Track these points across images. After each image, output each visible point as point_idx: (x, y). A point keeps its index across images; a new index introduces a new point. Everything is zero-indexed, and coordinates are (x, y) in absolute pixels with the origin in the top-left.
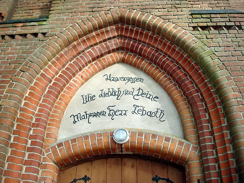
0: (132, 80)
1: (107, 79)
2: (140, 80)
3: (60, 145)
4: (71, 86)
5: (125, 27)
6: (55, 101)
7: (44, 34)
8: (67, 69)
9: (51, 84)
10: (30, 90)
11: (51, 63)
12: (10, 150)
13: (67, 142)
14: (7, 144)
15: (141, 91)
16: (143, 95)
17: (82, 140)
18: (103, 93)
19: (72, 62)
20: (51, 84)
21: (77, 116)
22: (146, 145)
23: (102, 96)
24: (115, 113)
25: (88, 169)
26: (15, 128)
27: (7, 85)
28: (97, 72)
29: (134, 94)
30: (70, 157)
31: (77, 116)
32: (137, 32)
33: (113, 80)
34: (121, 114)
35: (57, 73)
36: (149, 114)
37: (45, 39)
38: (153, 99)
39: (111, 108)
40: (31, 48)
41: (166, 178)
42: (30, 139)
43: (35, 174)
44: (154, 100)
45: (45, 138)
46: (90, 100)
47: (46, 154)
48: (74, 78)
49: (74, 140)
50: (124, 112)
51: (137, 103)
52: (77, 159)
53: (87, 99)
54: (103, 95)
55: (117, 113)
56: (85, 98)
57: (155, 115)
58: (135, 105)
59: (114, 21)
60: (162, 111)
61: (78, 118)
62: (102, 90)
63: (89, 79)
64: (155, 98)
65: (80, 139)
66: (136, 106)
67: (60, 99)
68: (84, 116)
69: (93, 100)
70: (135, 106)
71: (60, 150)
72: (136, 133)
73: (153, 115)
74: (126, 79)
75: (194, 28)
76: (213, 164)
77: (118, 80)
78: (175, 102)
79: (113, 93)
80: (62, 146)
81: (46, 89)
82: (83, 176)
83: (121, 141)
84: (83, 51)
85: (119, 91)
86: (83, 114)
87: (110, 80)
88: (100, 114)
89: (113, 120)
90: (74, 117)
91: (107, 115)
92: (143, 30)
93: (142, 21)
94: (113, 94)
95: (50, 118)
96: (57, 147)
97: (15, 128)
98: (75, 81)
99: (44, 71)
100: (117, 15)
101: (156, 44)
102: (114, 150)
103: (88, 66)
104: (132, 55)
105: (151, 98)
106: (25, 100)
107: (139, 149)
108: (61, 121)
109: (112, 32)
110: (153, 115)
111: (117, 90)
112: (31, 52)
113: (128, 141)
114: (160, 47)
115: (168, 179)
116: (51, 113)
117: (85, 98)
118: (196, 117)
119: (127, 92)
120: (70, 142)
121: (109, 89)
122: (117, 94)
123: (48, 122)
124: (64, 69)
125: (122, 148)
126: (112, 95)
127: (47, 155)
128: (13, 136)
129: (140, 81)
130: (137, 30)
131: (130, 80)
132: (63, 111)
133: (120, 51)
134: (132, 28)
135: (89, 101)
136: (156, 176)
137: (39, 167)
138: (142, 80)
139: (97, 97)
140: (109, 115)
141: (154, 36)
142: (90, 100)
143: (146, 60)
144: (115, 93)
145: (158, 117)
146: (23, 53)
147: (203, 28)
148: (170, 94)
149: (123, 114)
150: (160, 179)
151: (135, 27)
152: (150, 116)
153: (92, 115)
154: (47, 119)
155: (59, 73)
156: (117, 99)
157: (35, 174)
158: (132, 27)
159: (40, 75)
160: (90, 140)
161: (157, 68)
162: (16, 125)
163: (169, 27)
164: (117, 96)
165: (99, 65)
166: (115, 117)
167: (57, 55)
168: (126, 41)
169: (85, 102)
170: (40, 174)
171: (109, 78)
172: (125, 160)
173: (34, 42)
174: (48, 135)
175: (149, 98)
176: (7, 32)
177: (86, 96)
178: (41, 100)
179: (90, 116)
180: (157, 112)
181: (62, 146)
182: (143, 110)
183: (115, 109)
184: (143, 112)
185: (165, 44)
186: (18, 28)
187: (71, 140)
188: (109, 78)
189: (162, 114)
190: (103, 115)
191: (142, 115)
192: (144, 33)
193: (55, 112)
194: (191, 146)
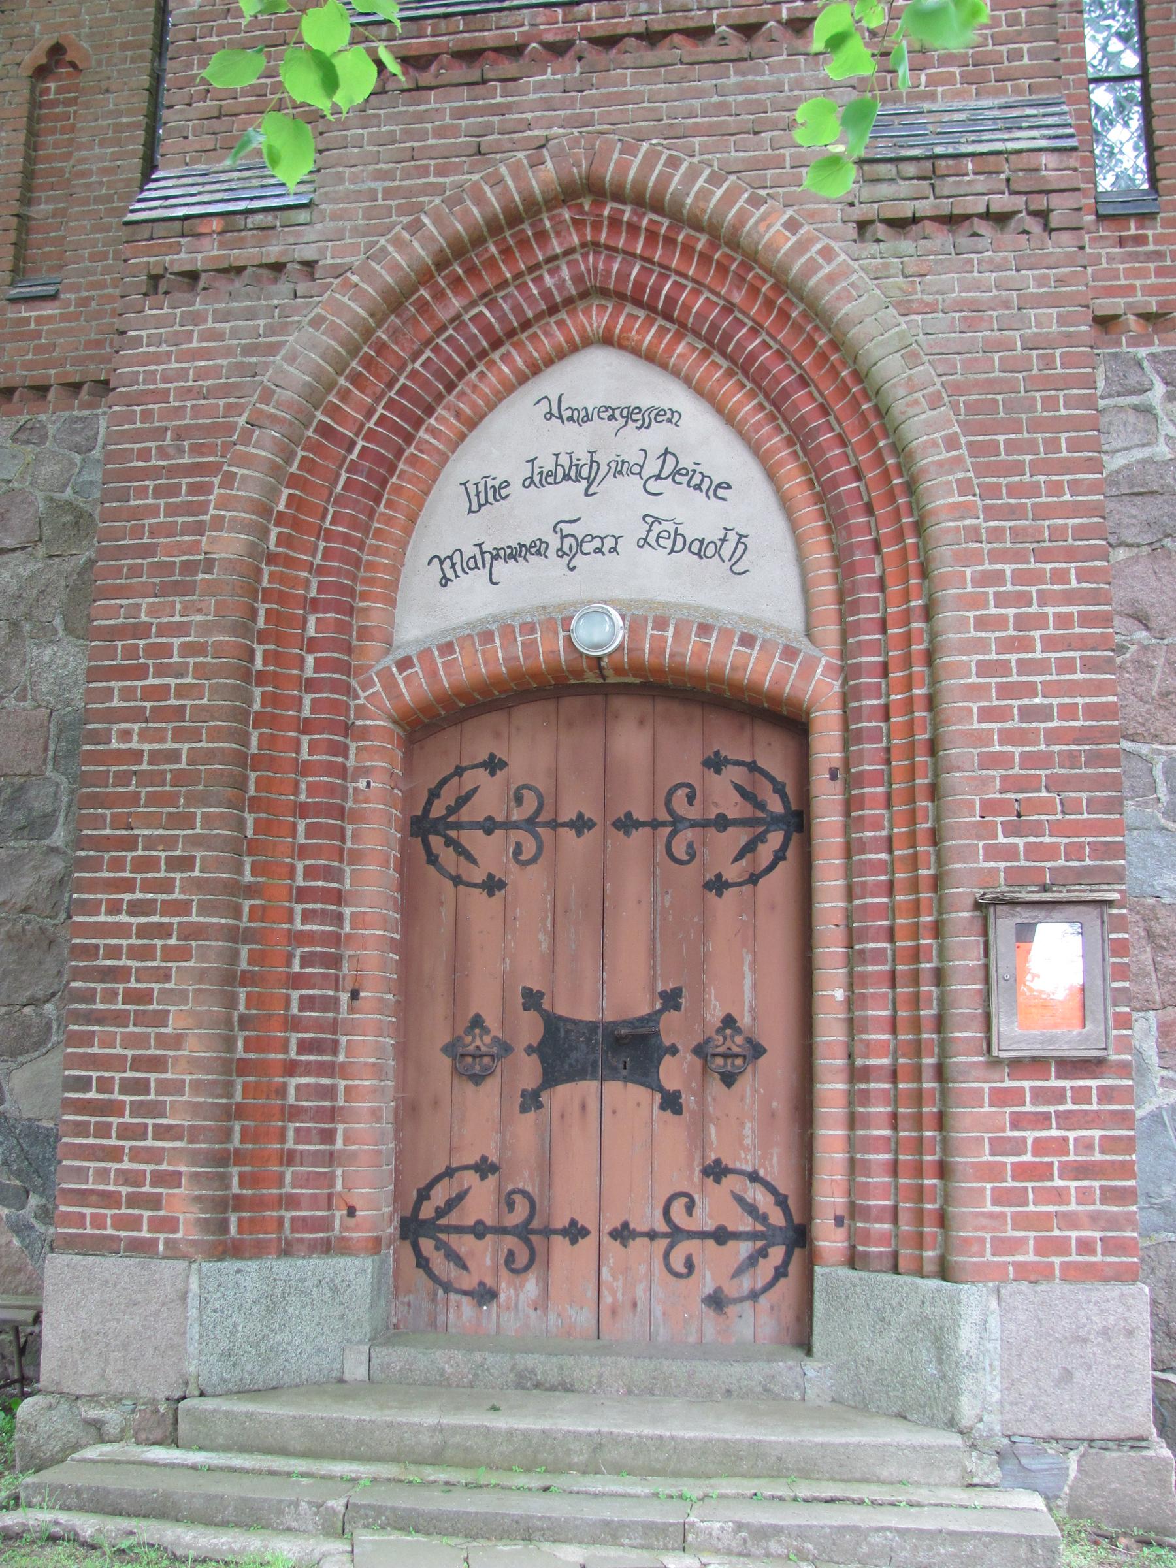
0: (639, 417)
1: (549, 415)
2: (669, 415)
3: (404, 664)
4: (422, 452)
5: (606, 213)
6: (371, 514)
7: (310, 265)
8: (404, 390)
9: (354, 456)
10: (288, 486)
11: (346, 379)
12: (257, 692)
13: (425, 654)
14: (246, 675)
15: (670, 460)
16: (678, 478)
17: (473, 644)
18: (537, 470)
19: (417, 365)
20: (354, 456)
21: (451, 558)
22: (678, 659)
23: (532, 482)
24: (580, 545)
25: (497, 735)
26: (261, 623)
27: (217, 480)
28: (510, 389)
29: (645, 475)
30: (439, 700)
31: (451, 558)
32: (652, 236)
33: (570, 419)
34: (599, 551)
35: (369, 414)
36: (696, 547)
37: (313, 287)
38: (711, 493)
39: (567, 529)
40: (271, 330)
41: (748, 759)
42: (309, 651)
43: (340, 759)
44: (715, 495)
45: (355, 643)
46: (491, 499)
47: (362, 695)
48: (432, 421)
49: (447, 648)
50: (610, 543)
51: (657, 508)
52: (462, 705)
53: (482, 496)
54: (536, 479)
55: (586, 547)
56: (473, 492)
57: (718, 551)
58: (647, 516)
59: (564, 192)
60: (741, 536)
61: (453, 566)
62: (532, 461)
63: (482, 417)
64: (719, 486)
65: (467, 643)
66: (650, 520)
67: (389, 504)
68: (474, 557)
69: (503, 498)
70: (649, 520)
71: (407, 680)
72: (646, 619)
73: (711, 550)
74: (617, 413)
75: (863, 226)
76: (874, 724)
77: (588, 419)
78: (786, 504)
79: (571, 473)
80: (412, 666)
81: (338, 476)
82: (483, 756)
83: (597, 647)
84: (458, 316)
85: (592, 461)
86: (470, 550)
87: (560, 417)
88: (528, 550)
89: (572, 569)
90: (442, 563)
91: (551, 553)
92: (675, 227)
93: (668, 196)
94: (573, 474)
95: (362, 573)
96: (394, 670)
97: (261, 623)
98: (433, 431)
99: (324, 413)
100: (575, 170)
101: (723, 285)
102: (578, 673)
103: (478, 370)
104: (637, 317)
105: (705, 487)
106: (278, 524)
107: (659, 671)
108: (398, 580)
109: (558, 234)
110: (711, 550)
111: (585, 459)
112: (273, 349)
113: (621, 647)
114: (737, 298)
115: (754, 762)
116: (365, 557)
117: (473, 492)
118: (844, 566)
119: (620, 469)
120: (436, 653)
121: (557, 455)
122: (585, 473)
123: (358, 588)
124: (392, 394)
125: (601, 669)
126: (567, 477)
127: (367, 698)
128: (259, 650)
129: (670, 421)
130: (653, 228)
131: (635, 417)
132: (403, 545)
133: (596, 302)
134: (635, 219)
135: (487, 502)
136: (717, 753)
137: (346, 736)
138: (676, 416)
139: (516, 489)
140: (561, 553)
141: (716, 257)
142: (491, 499)
143: (690, 338)
144: (579, 470)
145: (726, 558)
146: (248, 351)
147: (900, 225)
148: (771, 475)
149: (605, 550)
150: (727, 761)
151: (644, 214)
152: (698, 554)
153: (502, 553)
154: (354, 578)
155: (375, 410)
156: (586, 494)
157: (340, 759)
158: (634, 212)
159: (315, 431)
160: (498, 643)
161: (730, 373)
162: (262, 613)
163: (769, 227)
164: (584, 483)
165: (520, 362)
166: (579, 560)
167: (366, 349)
168: (616, 266)
169: (475, 507)
170: (352, 756)
171: (557, 414)
172: (619, 703)
173: (276, 302)
174: (364, 633)
175: (698, 487)
176: (167, 258)
177: (476, 484)
178: (329, 518)
179: (495, 557)
180: (724, 540)
181: (412, 666)
182: (676, 534)
183: (579, 530)
184: (677, 543)
185: (754, 291)
186: (206, 242)
187: (440, 648)
188: (555, 411)
189: (741, 547)
190: (538, 553)
191: (672, 551)
192: (680, 238)
193: (376, 551)
194: (823, 661)
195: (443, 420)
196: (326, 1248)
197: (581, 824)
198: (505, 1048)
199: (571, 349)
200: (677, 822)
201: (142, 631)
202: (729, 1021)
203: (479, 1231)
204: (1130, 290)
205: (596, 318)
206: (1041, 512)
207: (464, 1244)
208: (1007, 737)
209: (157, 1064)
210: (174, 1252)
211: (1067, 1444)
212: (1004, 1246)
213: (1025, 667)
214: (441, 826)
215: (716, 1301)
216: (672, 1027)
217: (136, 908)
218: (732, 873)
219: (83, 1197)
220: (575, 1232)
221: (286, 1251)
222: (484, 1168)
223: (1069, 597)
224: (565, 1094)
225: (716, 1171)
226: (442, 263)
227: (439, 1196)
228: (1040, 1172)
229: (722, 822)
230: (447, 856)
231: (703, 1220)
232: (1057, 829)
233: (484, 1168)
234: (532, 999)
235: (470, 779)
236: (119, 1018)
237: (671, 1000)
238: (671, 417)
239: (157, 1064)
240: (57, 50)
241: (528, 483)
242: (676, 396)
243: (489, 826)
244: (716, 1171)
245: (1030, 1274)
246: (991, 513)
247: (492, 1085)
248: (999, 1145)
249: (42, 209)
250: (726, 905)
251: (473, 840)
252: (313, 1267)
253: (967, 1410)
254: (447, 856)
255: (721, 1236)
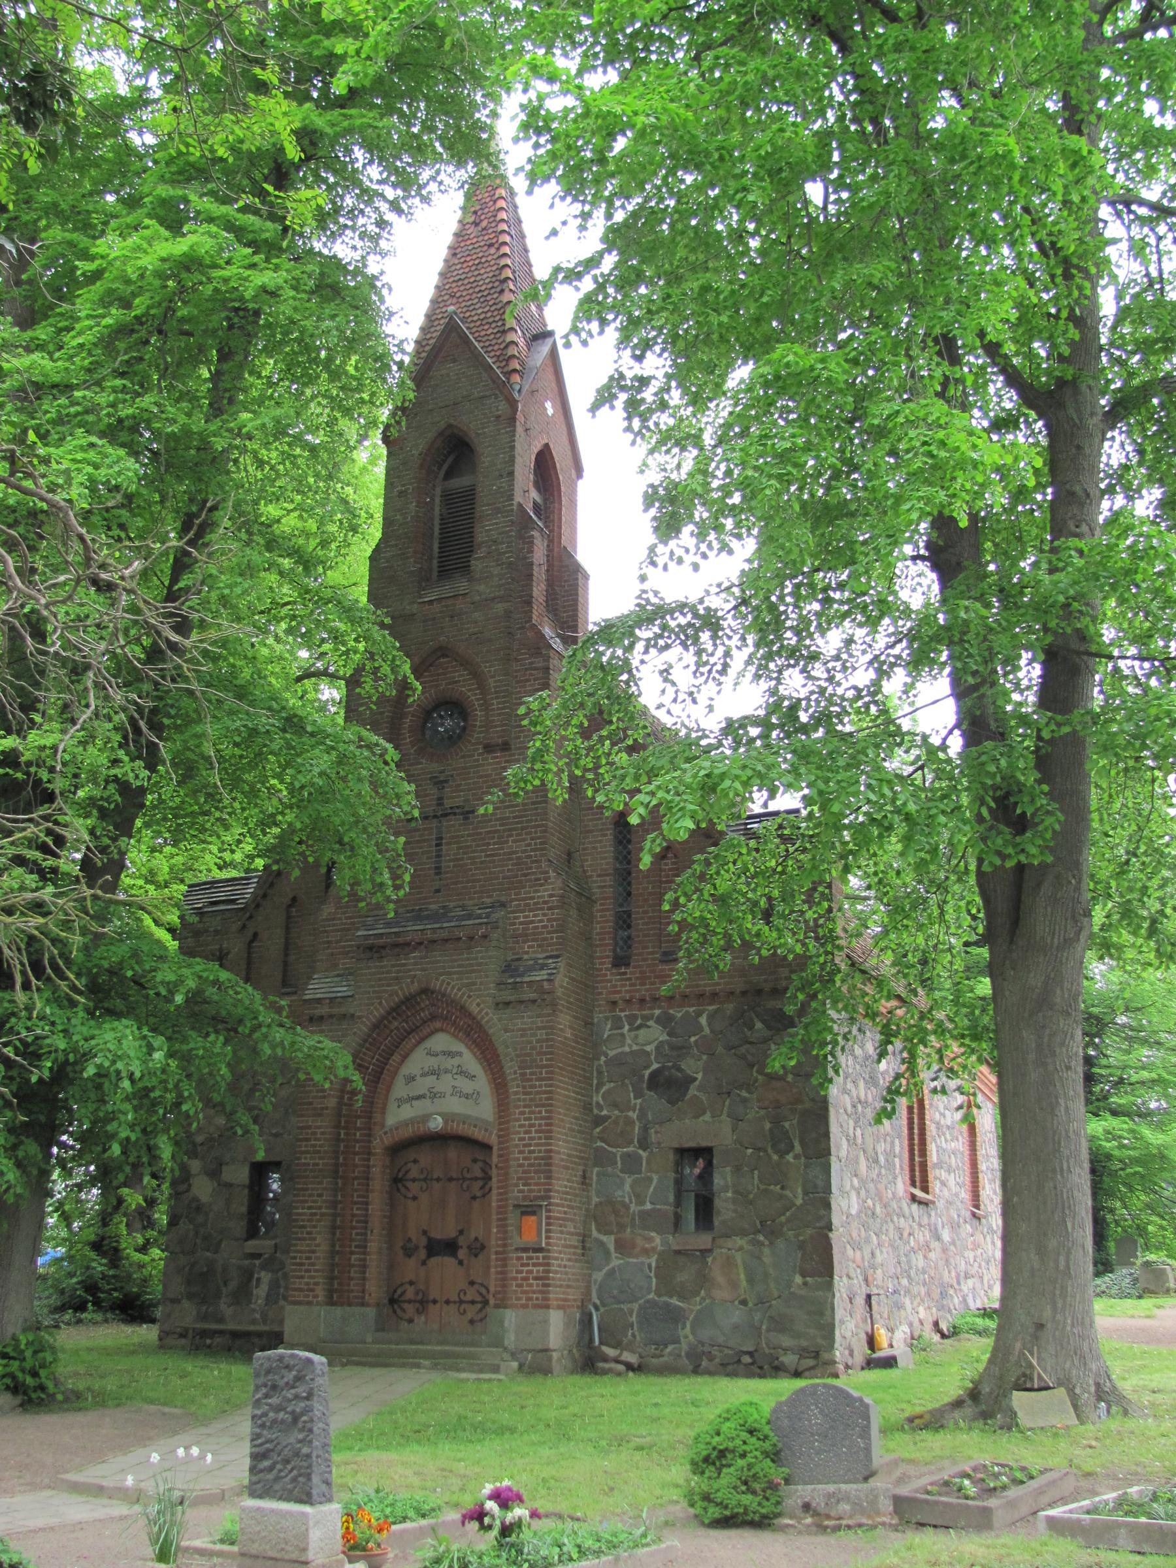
51: (456, 1083)
66: (454, 1087)
119: (446, 1071)
147: (507, 1004)
195: (396, 1057)
196: (363, 1305)
197: (438, 1180)
198: (417, 1248)
199: (432, 1033)
200: (464, 1179)
201: (309, 1127)
202: (476, 1239)
203: (409, 1302)
204: (619, 992)
205: (438, 1024)
206: (539, 1093)
207: (405, 1306)
208: (525, 1159)
209: (313, 1252)
210: (318, 1304)
211: (529, 1351)
212: (518, 1299)
213: (531, 1139)
214: (401, 1180)
215: (472, 1322)
216: (462, 1241)
217: (310, 1208)
218: (479, 1194)
219: (295, 1290)
220: (435, 1302)
221: (350, 1305)
222: (411, 1283)
223: (542, 1118)
224: (434, 1260)
225: (472, 1283)
226: (389, 1013)
227: (399, 1291)
228: (526, 1279)
229: (476, 1179)
230: (403, 1190)
231: (469, 1297)
232: (536, 1184)
233: (411, 1283)
234: (425, 1233)
235: (410, 1165)
236: (304, 1239)
237: (461, 1232)
238: (460, 1054)
239: (313, 1252)
240: (294, 899)
241: (422, 1075)
242: (461, 1048)
243: (414, 1180)
244: (472, 1283)
245: (525, 1306)
246: (525, 1093)
247: (413, 1259)
248: (518, 1272)
249: (292, 958)
250: (476, 1204)
251: (409, 1184)
252: (357, 1310)
253: (506, 1343)
254: (403, 1190)
255: (473, 1302)
